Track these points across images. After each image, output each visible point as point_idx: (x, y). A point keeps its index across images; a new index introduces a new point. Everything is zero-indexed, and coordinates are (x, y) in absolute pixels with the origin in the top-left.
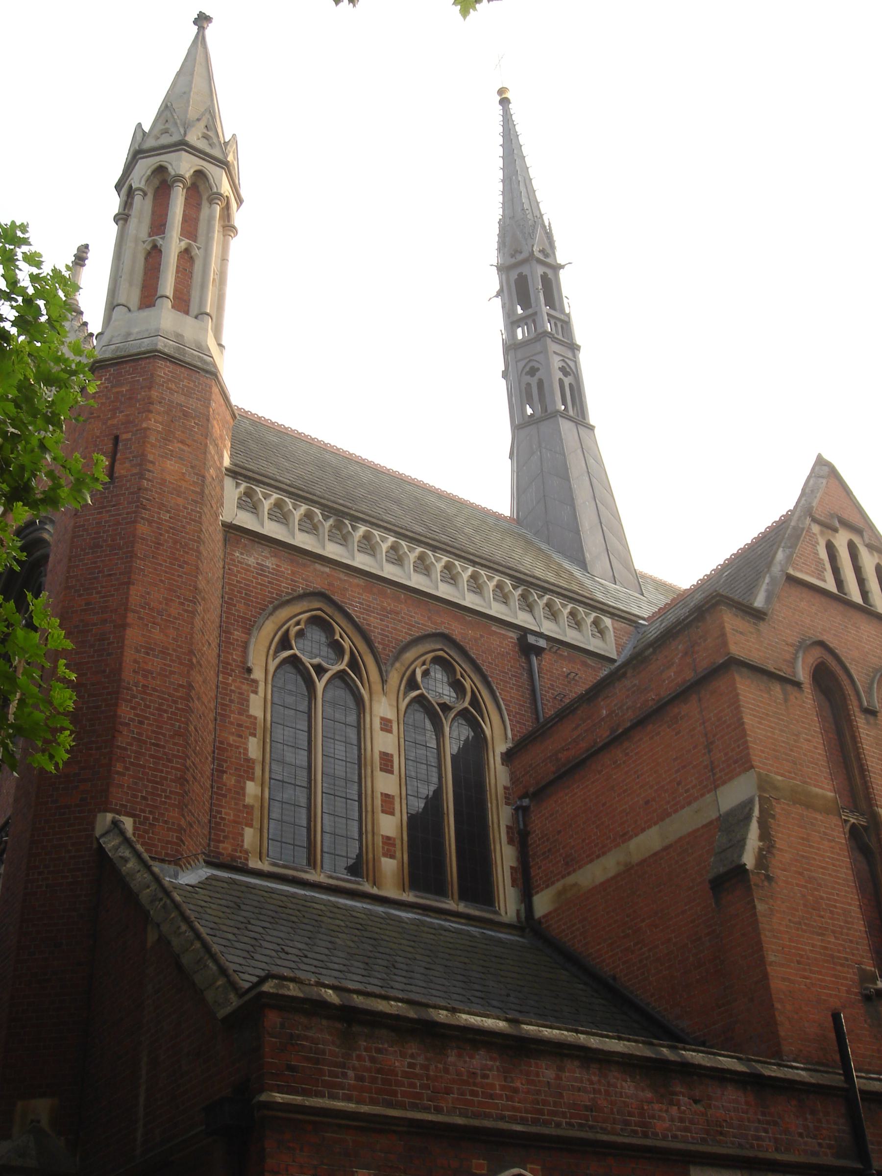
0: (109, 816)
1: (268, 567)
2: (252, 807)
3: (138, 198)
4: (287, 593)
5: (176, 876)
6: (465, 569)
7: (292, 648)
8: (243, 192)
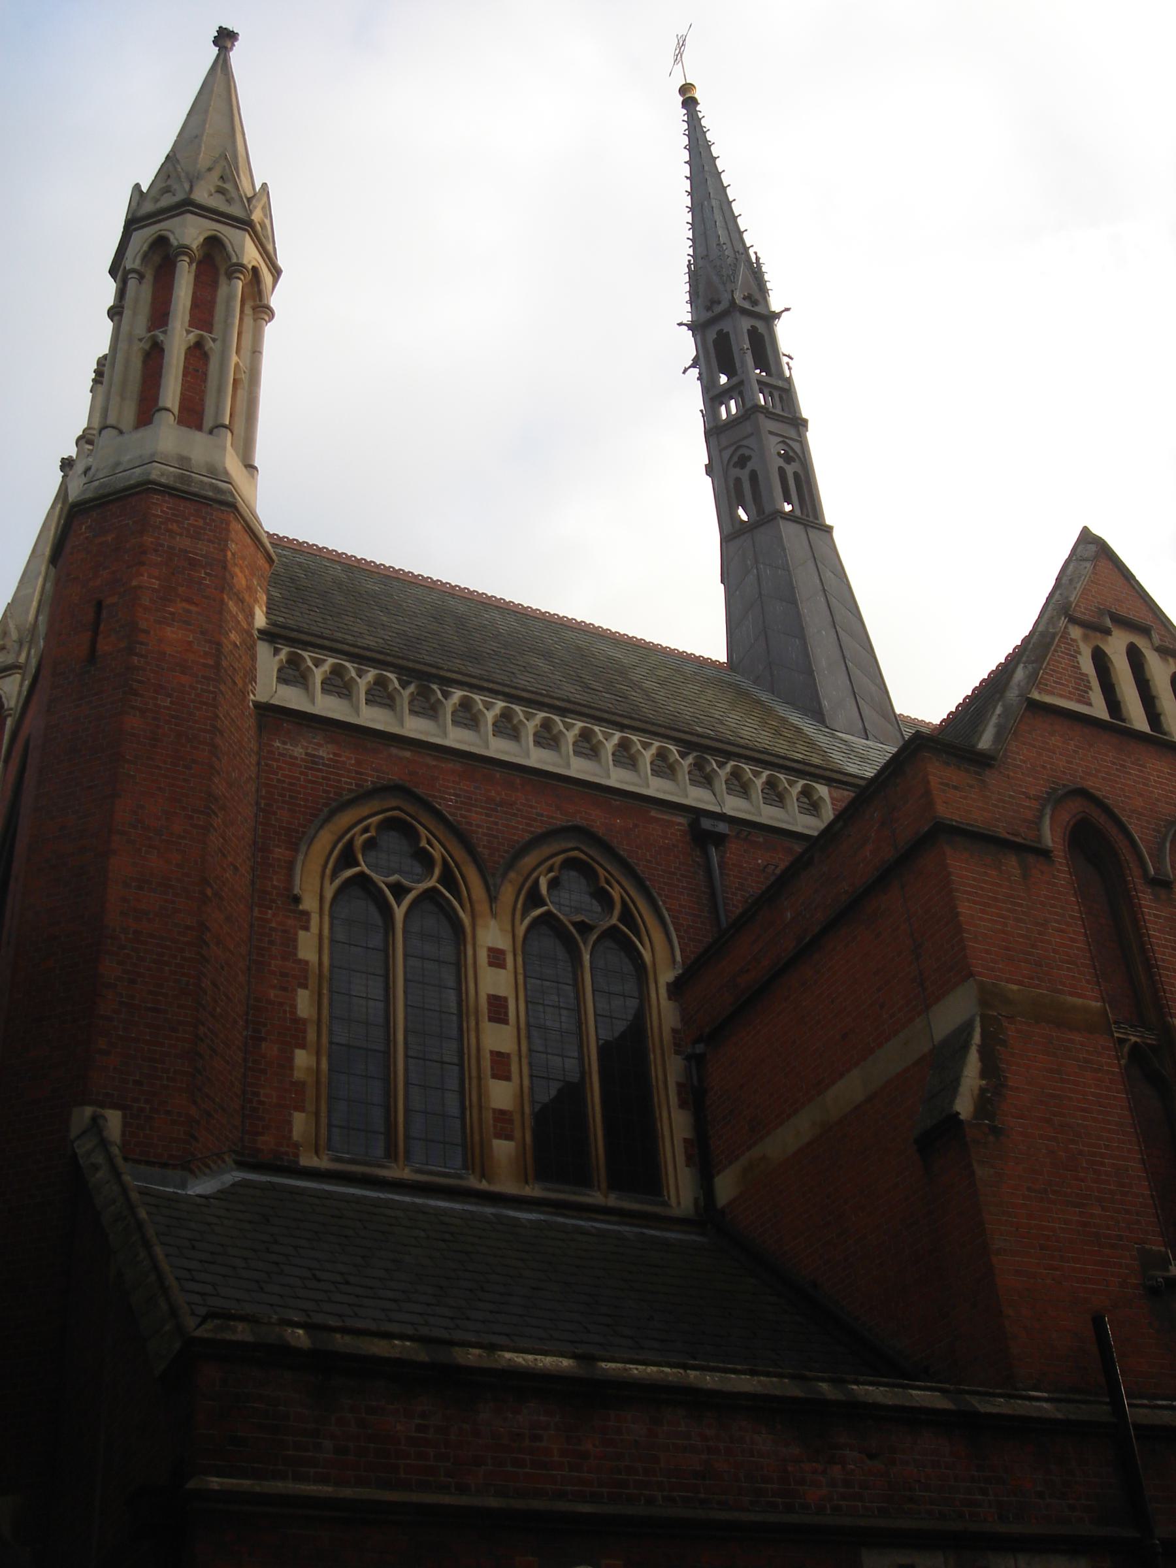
0: (88, 1111)
1: (322, 758)
2: (304, 1084)
3: (132, 283)
4: (350, 791)
5: (183, 1186)
6: (608, 737)
7: (358, 865)
8: (281, 262)
